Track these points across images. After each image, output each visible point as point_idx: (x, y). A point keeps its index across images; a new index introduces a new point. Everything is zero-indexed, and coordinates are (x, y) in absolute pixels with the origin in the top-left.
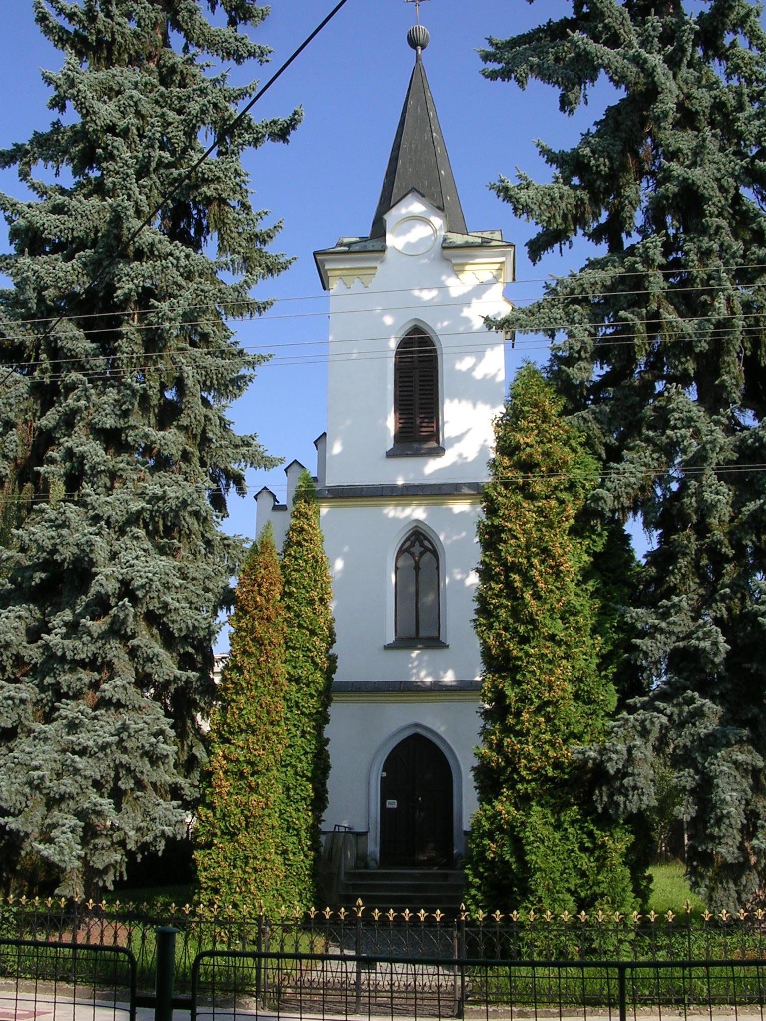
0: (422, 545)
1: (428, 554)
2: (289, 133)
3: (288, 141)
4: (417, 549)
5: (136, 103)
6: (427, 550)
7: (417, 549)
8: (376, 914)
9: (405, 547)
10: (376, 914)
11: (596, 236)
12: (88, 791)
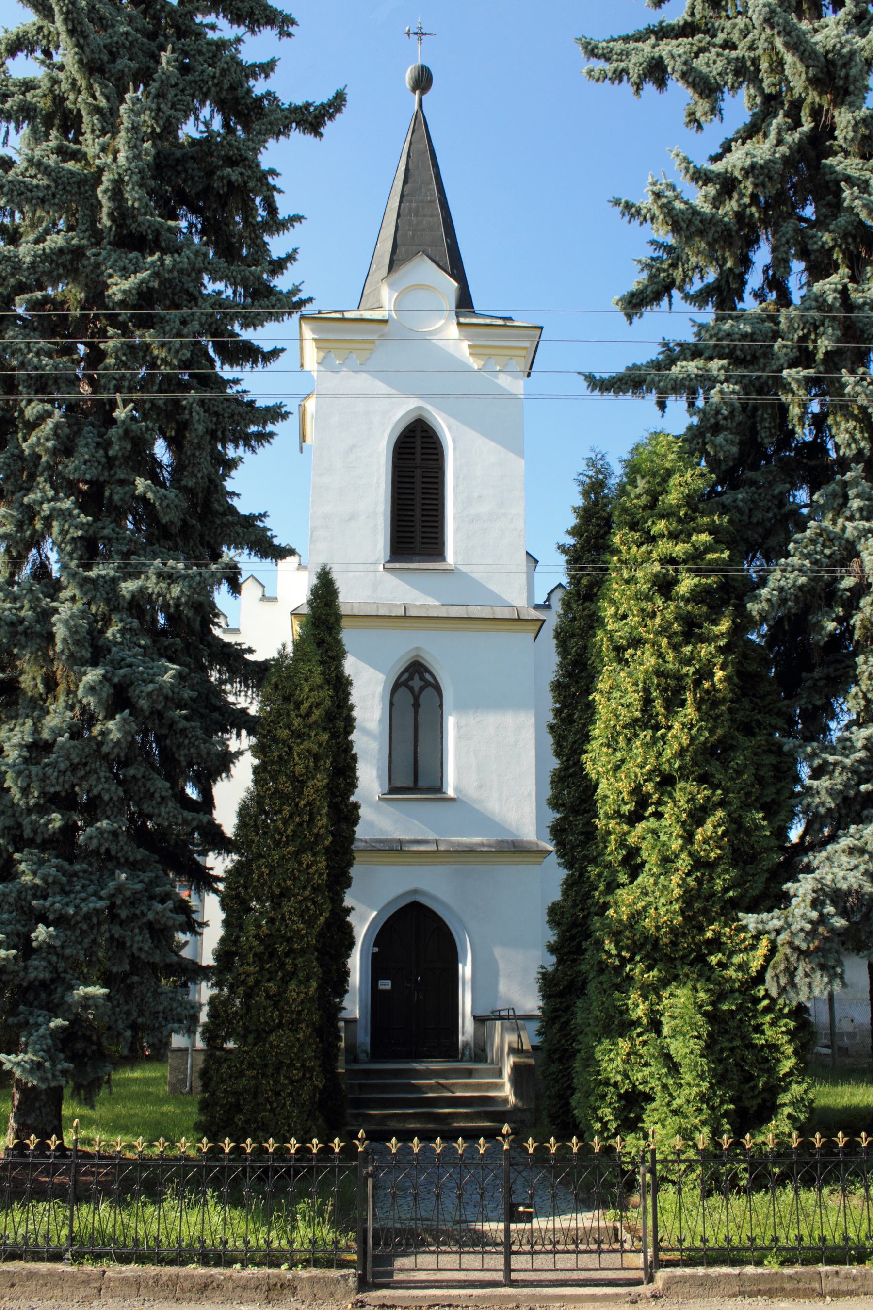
0: (422, 678)
1: (430, 690)
2: (323, 124)
3: (321, 135)
4: (416, 683)
5: (131, 43)
6: (428, 684)
7: (416, 683)
8: (531, 1145)
9: (402, 679)
10: (531, 1145)
11: (700, 299)
12: (69, 976)
